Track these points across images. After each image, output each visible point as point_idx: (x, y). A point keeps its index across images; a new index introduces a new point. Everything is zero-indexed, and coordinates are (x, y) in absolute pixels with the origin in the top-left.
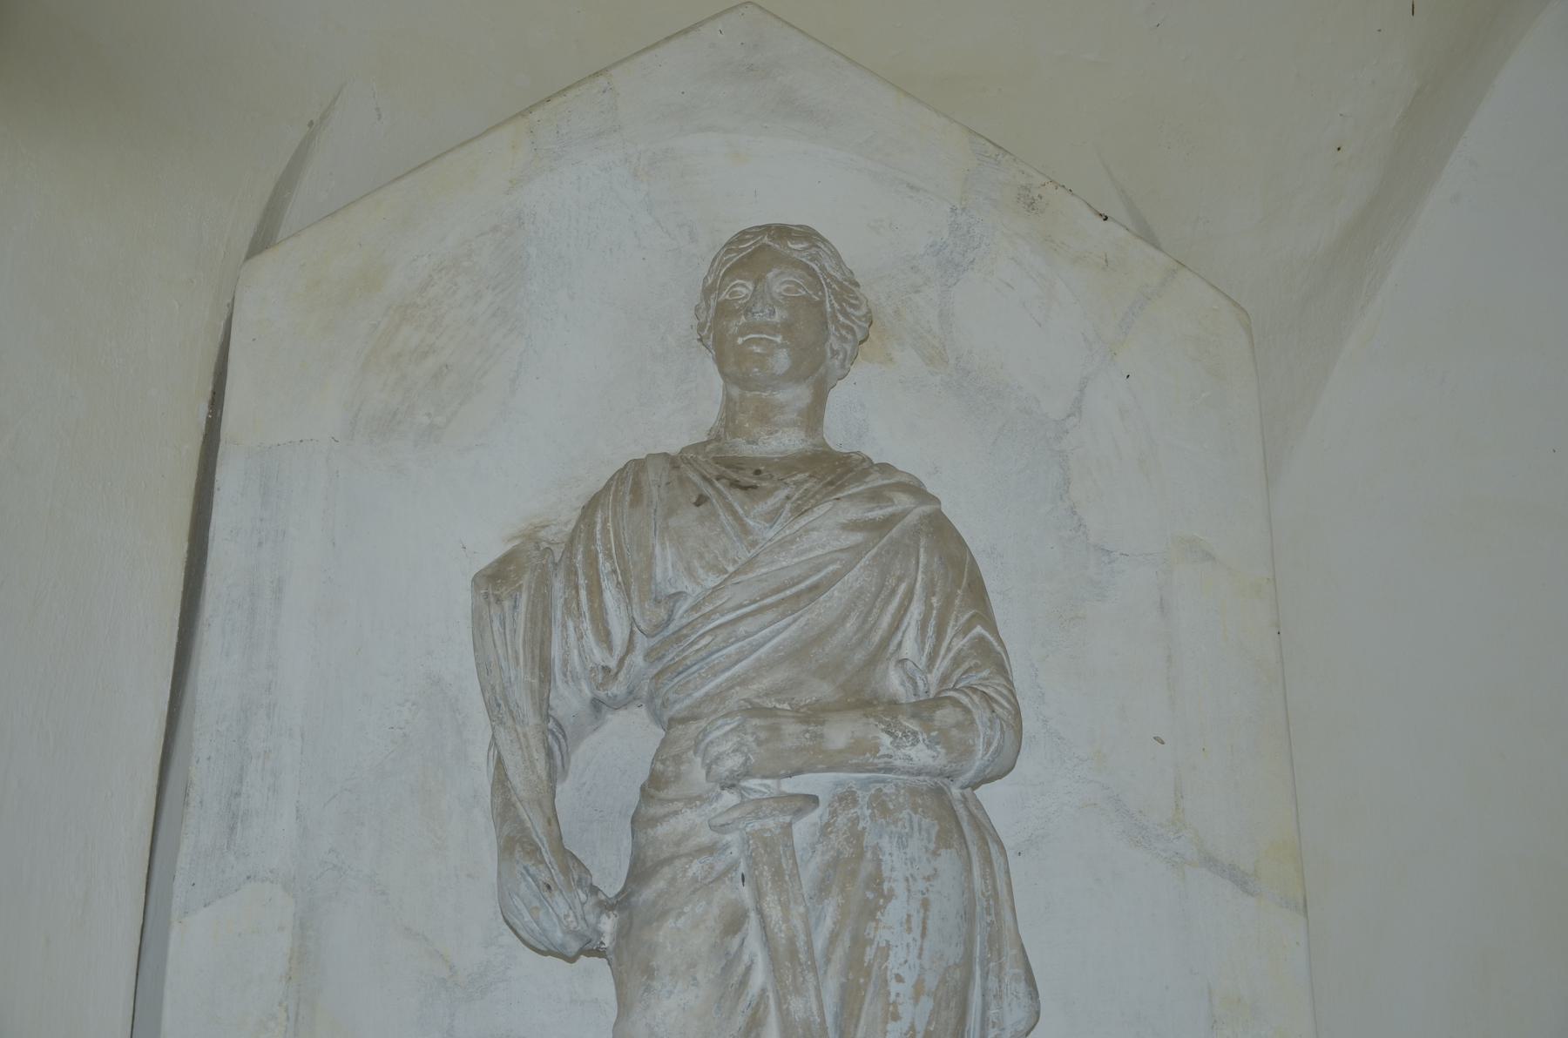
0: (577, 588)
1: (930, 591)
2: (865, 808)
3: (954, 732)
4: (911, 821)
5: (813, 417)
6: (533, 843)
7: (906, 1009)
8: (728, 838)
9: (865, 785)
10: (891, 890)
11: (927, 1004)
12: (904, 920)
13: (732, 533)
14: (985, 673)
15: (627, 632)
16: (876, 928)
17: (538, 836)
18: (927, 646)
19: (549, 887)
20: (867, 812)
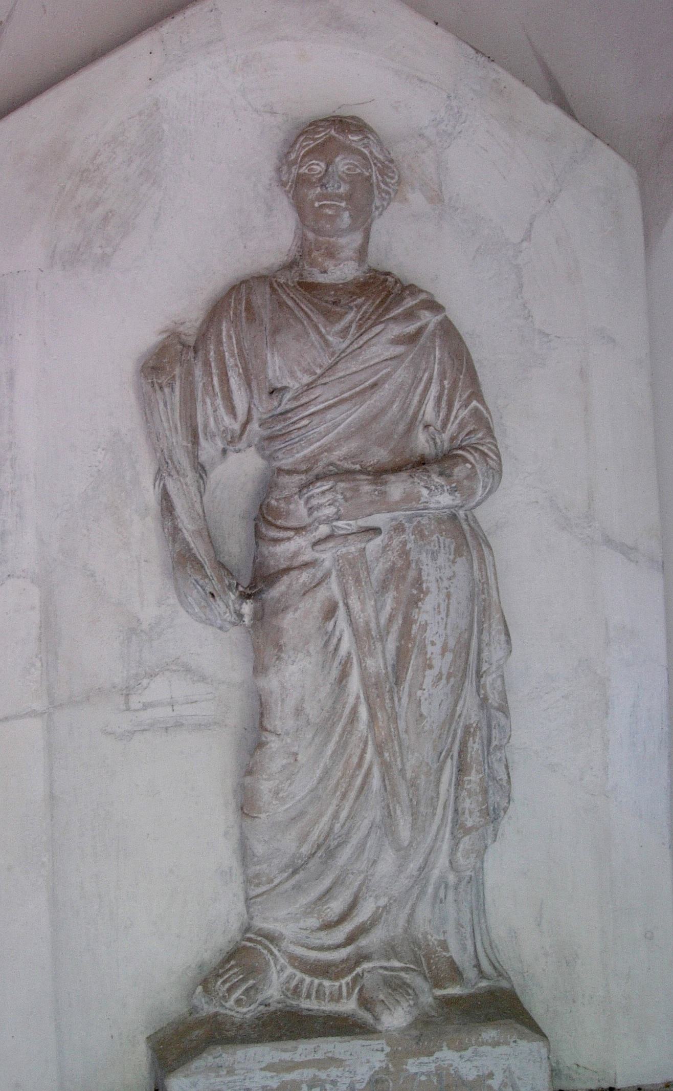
0: (211, 375)
1: (442, 375)
2: (411, 534)
3: (465, 482)
4: (439, 542)
5: (362, 252)
6: (199, 563)
7: (437, 662)
8: (323, 556)
9: (410, 519)
10: (428, 588)
11: (449, 656)
12: (436, 607)
13: (318, 346)
14: (480, 435)
15: (246, 406)
16: (419, 613)
17: (201, 557)
18: (441, 414)
19: (213, 595)
20: (412, 537)
